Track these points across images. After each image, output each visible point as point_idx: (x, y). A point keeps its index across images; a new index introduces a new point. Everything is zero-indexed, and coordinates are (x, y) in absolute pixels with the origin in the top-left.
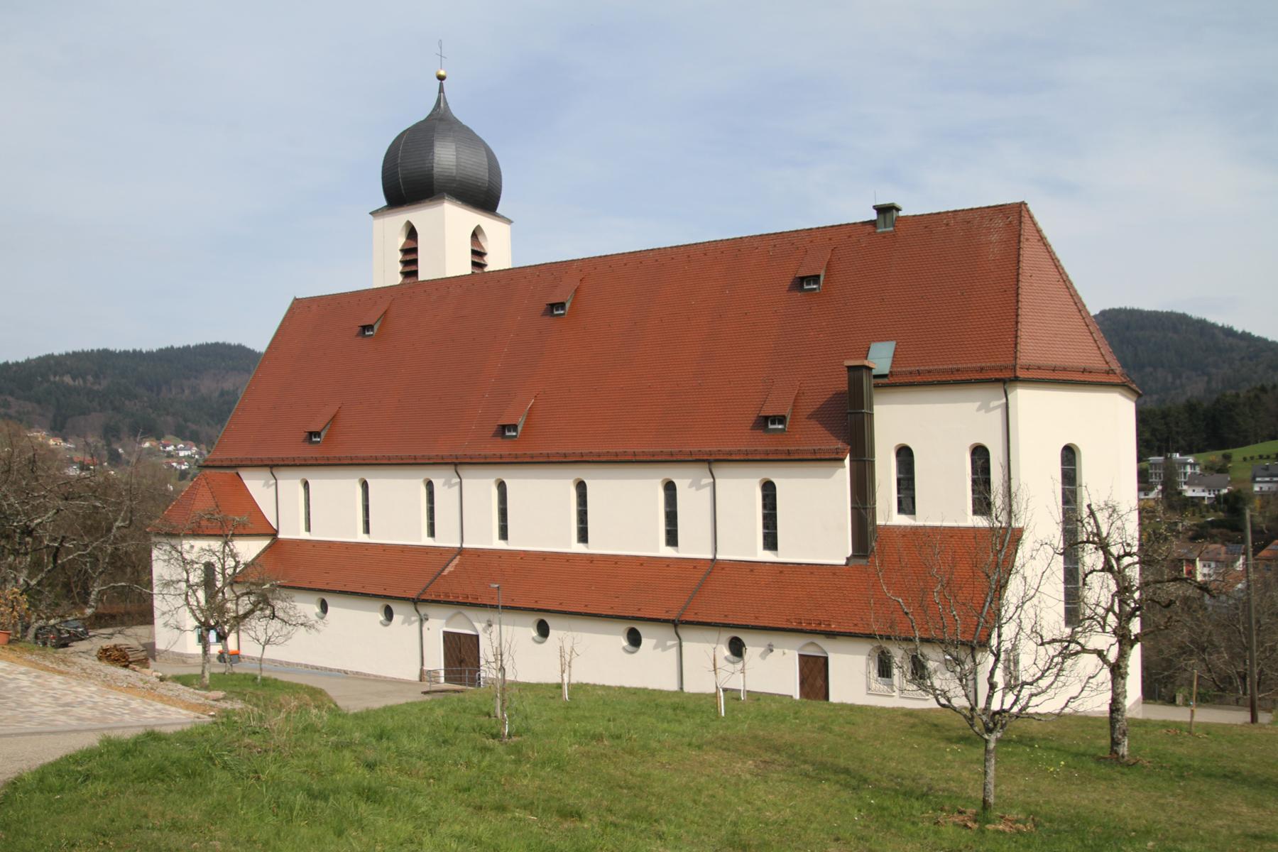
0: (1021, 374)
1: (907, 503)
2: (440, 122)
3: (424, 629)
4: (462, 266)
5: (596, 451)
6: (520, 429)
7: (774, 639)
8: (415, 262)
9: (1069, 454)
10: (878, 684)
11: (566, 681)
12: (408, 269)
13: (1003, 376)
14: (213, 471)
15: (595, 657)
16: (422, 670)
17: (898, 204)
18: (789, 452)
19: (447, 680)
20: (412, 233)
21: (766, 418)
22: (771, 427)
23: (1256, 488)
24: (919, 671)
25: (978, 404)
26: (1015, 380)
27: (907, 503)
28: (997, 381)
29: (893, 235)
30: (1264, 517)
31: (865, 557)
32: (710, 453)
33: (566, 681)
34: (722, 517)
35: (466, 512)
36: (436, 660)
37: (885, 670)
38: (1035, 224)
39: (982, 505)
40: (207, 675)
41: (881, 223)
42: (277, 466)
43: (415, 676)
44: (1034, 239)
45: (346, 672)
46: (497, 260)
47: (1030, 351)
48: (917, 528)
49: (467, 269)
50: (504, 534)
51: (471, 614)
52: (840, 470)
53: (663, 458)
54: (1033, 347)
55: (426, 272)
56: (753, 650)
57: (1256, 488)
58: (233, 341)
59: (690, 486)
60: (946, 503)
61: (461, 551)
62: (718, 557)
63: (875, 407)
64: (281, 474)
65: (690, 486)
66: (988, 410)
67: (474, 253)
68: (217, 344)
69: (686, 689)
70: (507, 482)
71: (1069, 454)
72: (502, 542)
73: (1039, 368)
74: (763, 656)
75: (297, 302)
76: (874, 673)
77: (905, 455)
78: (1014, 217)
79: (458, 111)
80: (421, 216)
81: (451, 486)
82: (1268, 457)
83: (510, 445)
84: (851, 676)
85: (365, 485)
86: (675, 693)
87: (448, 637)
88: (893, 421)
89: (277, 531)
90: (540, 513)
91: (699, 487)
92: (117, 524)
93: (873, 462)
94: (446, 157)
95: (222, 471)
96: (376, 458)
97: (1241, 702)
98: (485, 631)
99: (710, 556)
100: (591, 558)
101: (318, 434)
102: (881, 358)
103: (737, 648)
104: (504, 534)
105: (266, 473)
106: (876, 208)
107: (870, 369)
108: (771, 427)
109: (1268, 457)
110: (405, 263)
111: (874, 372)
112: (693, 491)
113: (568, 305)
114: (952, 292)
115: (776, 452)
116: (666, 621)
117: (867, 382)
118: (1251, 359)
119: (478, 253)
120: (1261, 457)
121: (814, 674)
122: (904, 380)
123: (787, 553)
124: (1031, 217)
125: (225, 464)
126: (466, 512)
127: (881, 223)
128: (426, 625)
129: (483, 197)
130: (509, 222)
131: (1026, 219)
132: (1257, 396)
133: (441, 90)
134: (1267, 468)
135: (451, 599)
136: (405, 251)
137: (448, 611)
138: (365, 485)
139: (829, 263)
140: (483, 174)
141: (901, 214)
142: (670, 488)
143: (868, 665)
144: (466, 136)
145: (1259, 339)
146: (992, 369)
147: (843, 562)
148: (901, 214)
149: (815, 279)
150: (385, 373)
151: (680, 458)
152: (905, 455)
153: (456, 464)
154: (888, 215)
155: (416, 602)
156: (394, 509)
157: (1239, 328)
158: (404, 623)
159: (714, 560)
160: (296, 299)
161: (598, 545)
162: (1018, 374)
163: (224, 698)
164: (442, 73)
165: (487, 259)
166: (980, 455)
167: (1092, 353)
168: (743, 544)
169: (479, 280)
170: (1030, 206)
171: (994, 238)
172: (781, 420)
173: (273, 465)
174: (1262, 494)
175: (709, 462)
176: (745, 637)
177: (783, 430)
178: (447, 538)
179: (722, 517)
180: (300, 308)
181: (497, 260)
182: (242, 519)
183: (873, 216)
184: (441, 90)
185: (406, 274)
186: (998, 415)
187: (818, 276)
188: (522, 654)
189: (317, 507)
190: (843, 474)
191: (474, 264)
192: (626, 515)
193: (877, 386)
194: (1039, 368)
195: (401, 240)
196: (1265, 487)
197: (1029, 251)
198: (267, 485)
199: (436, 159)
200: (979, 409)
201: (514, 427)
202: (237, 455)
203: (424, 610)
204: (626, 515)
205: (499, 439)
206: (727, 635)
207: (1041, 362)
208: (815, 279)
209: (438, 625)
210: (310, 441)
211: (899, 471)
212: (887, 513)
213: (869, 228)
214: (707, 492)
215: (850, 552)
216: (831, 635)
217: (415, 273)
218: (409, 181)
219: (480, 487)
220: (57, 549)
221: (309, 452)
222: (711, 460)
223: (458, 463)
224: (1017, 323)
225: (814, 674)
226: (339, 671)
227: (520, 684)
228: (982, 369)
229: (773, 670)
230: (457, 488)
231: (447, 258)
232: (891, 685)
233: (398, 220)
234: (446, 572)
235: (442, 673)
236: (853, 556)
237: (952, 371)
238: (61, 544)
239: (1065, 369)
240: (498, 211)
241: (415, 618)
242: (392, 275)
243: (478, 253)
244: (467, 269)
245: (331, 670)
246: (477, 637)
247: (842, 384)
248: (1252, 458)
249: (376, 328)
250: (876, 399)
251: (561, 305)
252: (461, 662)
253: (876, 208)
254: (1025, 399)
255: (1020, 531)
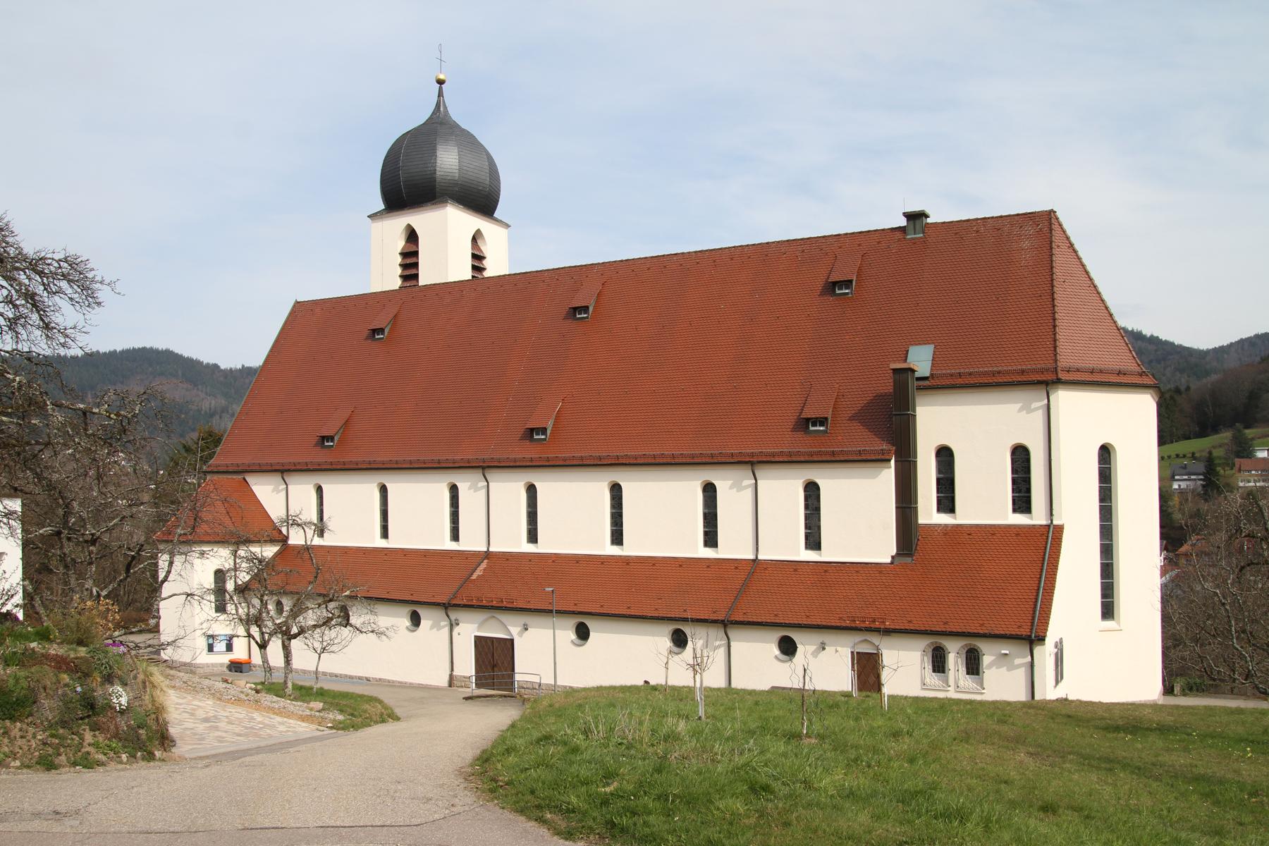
0: (1062, 376)
1: (947, 502)
2: (439, 126)
3: (455, 634)
4: (461, 271)
5: (528, 456)
6: (549, 432)
7: (827, 637)
8: (416, 265)
9: (1106, 453)
10: (933, 679)
11: (698, 685)
12: (408, 272)
13: (1045, 378)
14: (221, 476)
15: (628, 657)
16: (451, 676)
17: (928, 211)
18: (833, 453)
19: (478, 686)
20: (412, 236)
21: (808, 420)
22: (812, 428)
23: (1175, 486)
24: (973, 665)
25: (1019, 405)
26: (1058, 382)
27: (947, 502)
28: (1039, 383)
29: (924, 241)
30: (1183, 514)
31: (910, 555)
32: (752, 455)
33: (698, 685)
34: (763, 517)
35: (494, 514)
36: (467, 665)
37: (939, 665)
38: (1064, 232)
39: (1022, 502)
40: (290, 685)
41: (910, 229)
42: (289, 471)
43: (443, 681)
44: (1064, 246)
45: (368, 680)
46: (495, 267)
47: (1069, 355)
48: (958, 526)
49: (467, 274)
50: (385, 534)
51: (506, 618)
52: (886, 471)
53: (665, 461)
54: (1073, 349)
55: (427, 276)
56: (806, 645)
57: (1175, 486)
58: (161, 345)
59: (731, 488)
60: (984, 501)
61: (488, 555)
62: (760, 557)
63: (919, 410)
64: (291, 479)
65: (731, 488)
66: (1030, 411)
67: (475, 257)
68: (144, 349)
69: (733, 685)
70: (539, 486)
71: (1106, 453)
72: (454, 543)
73: (1078, 370)
74: (815, 654)
75: (298, 306)
76: (929, 667)
77: (945, 456)
78: (1043, 226)
79: (458, 113)
80: (422, 220)
81: (477, 489)
82: (1184, 456)
83: (539, 449)
84: (905, 669)
85: (319, 490)
86: (1024, 705)
87: (479, 641)
88: (934, 421)
89: (287, 538)
90: (573, 513)
91: (740, 489)
92: (179, 531)
93: (915, 462)
94: (448, 160)
95: (225, 476)
96: (397, 462)
97: (1236, 691)
98: (520, 634)
99: (752, 557)
100: (627, 561)
101: (331, 438)
102: (921, 359)
103: (788, 648)
104: (385, 534)
105: (276, 479)
106: (904, 214)
107: (913, 371)
108: (812, 428)
109: (1184, 456)
110: (404, 266)
111: (917, 375)
112: (733, 492)
113: (591, 309)
114: (991, 297)
115: (820, 453)
116: (715, 622)
117: (912, 384)
118: (1159, 362)
119: (478, 257)
120: (1177, 456)
121: (868, 670)
122: (949, 382)
123: (831, 552)
124: (1060, 225)
125: (221, 469)
126: (494, 514)
127: (910, 229)
128: (456, 630)
129: (481, 199)
130: (507, 226)
131: (1055, 227)
132: (1172, 398)
133: (440, 94)
134: (1185, 467)
135: (484, 603)
136: (404, 255)
137: (480, 616)
138: (319, 490)
139: (860, 269)
140: (485, 177)
141: (929, 220)
142: (454, 490)
143: (923, 661)
144: (468, 142)
145: (1166, 343)
146: (1034, 371)
147: (889, 560)
148: (929, 220)
149: (848, 283)
150: (380, 376)
151: (720, 460)
152: (945, 456)
153: (483, 468)
154: (918, 222)
155: (447, 607)
156: (418, 515)
157: (1147, 332)
158: (433, 627)
159: (754, 561)
160: (297, 302)
161: (633, 547)
162: (1060, 376)
163: (323, 709)
164: (442, 77)
165: (486, 263)
166: (1021, 456)
167: (1125, 360)
168: (784, 543)
169: (480, 286)
170: (1058, 214)
171: (1026, 244)
172: (823, 421)
173: (284, 470)
174: (1181, 492)
175: (752, 464)
176: (796, 636)
177: (825, 432)
178: (472, 541)
179: (763, 517)
180: (301, 311)
181: (495, 267)
182: (247, 526)
183: (903, 222)
184: (440, 94)
185: (405, 278)
186: (1039, 416)
187: (851, 281)
188: (546, 655)
189: (343, 513)
190: (888, 475)
191: (474, 268)
192: (663, 516)
193: (919, 388)
194: (1078, 370)
195: (401, 244)
196: (1183, 485)
197: (1060, 258)
198: (277, 491)
199: (439, 162)
200: (1020, 410)
201: (544, 431)
202: (246, 460)
203: (453, 615)
204: (663, 516)
205: (528, 443)
206: (777, 635)
207: (1080, 365)
208: (848, 283)
209: (469, 629)
210: (323, 446)
211: (939, 471)
212: (928, 513)
213: (899, 235)
214: (749, 493)
215: (894, 552)
216: (888, 632)
217: (416, 277)
218: (408, 184)
219: (508, 491)
220: (133, 557)
221: (320, 457)
222: (753, 462)
223: (485, 466)
224: (1055, 326)
225: (868, 670)
226: (360, 678)
227: (674, 688)
228: (1023, 372)
229: (827, 667)
230: (484, 492)
231: (445, 263)
232: (946, 682)
233: (397, 225)
234: (474, 577)
235: (474, 679)
236: (898, 554)
237: (993, 374)
238: (138, 553)
239: (1101, 372)
240: (496, 215)
241: (445, 623)
242: (391, 280)
243: (478, 257)
244: (467, 274)
245: (351, 677)
246: (512, 641)
247: (887, 385)
248: (1169, 457)
249: (386, 331)
250: (918, 401)
251: (585, 309)
252: (494, 666)
253: (904, 214)
254: (1064, 399)
255: (1059, 529)
